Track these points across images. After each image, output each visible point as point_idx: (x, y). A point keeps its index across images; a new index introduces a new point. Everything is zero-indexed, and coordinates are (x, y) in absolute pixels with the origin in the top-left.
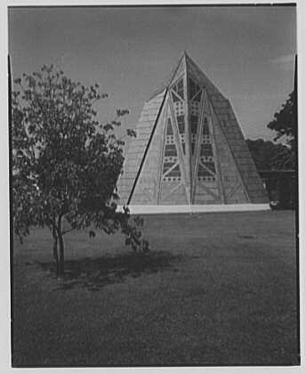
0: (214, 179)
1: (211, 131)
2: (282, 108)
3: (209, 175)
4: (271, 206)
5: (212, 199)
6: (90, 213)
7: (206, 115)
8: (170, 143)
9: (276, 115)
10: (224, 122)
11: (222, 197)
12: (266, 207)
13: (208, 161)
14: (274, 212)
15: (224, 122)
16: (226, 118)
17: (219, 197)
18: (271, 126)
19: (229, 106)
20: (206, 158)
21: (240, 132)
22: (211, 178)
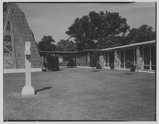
0: (11, 55)
1: (12, 29)
2: (71, 25)
3: (8, 52)
4: (42, 69)
5: (9, 66)
6: (116, 32)
7: (9, 20)
8: (8, 35)
9: (115, 13)
10: (20, 24)
11: (15, 65)
12: (40, 70)
13: (8, 45)
14: (44, 72)
15: (20, 24)
16: (22, 23)
17: (13, 65)
18: (67, 33)
19: (24, 16)
20: (7, 43)
21: (31, 82)
22: (9, 54)
